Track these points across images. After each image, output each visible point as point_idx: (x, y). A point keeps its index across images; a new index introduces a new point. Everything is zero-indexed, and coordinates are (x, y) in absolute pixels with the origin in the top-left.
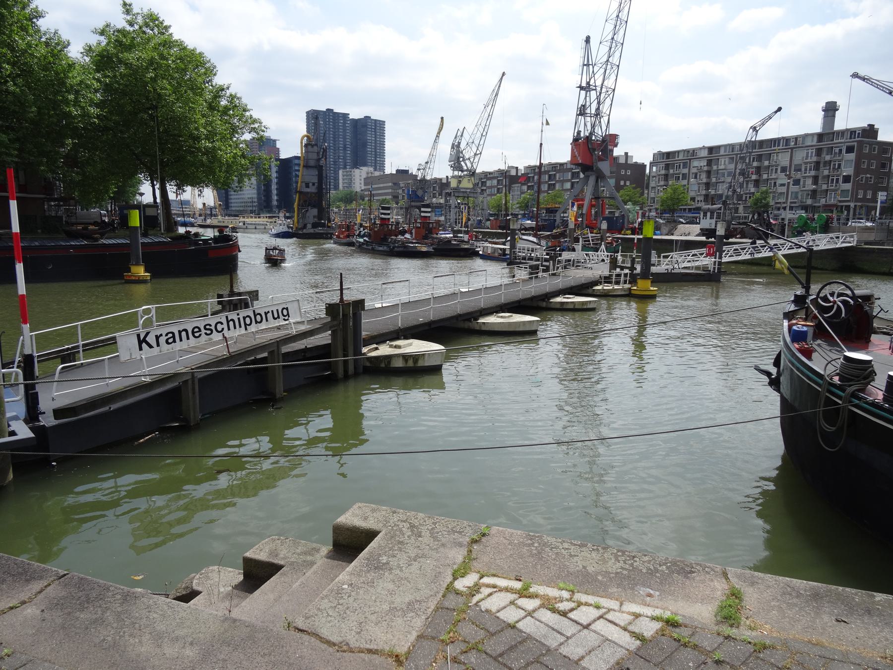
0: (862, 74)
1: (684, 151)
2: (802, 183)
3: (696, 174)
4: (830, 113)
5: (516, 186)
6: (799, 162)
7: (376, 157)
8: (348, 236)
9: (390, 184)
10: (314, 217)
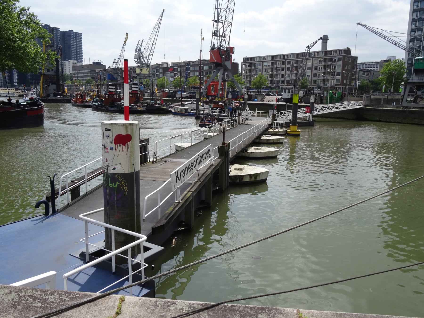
0: (362, 23)
1: (259, 57)
2: (318, 75)
3: (266, 69)
4: (325, 41)
5: (167, 74)
6: (317, 65)
7: (77, 54)
8: (82, 102)
9: (90, 71)
10: (54, 90)
